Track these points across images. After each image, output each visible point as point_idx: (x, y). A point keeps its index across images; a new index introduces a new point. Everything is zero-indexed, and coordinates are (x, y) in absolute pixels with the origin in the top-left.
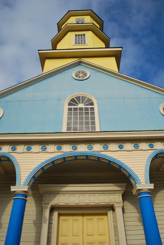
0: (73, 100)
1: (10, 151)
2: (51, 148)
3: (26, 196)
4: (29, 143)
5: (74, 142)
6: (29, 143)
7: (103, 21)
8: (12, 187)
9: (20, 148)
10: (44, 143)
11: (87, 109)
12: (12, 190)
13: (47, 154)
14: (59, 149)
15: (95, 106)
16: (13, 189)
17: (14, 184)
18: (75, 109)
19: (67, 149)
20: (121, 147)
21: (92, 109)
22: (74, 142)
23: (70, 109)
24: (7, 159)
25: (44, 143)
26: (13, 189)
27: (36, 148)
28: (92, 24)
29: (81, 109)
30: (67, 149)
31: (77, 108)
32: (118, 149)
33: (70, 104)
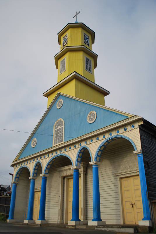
1: (117, 134)
2: (101, 138)
3: (78, 170)
4: (91, 138)
5: (110, 131)
6: (91, 138)
7: (82, 23)
8: (134, 152)
9: (89, 142)
10: (97, 136)
12: (29, 178)
13: (93, 143)
14: (104, 137)
16: (90, 163)
17: (30, 176)
19: (108, 136)
20: (125, 129)
22: (110, 131)
24: (108, 143)
25: (97, 136)
26: (90, 163)
27: (94, 140)
28: (82, 24)
30: (108, 136)
32: (132, 129)
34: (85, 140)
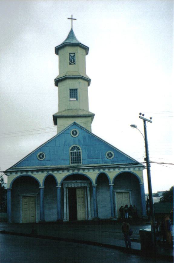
0: (72, 148)
11: (78, 152)
23: (71, 153)
29: (75, 152)
34: (53, 170)
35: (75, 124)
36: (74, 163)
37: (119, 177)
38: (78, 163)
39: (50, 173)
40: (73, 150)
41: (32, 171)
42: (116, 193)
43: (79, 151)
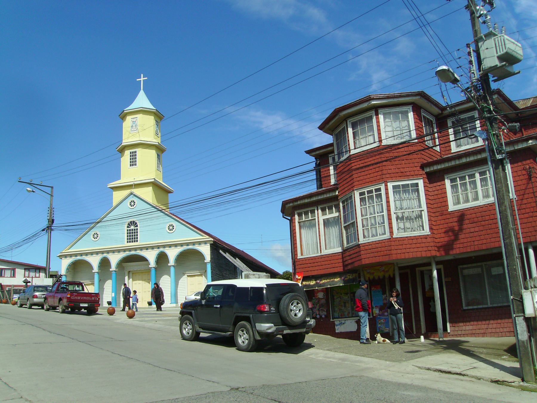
8: (93, 271)
11: (135, 230)
15: (138, 228)
18: (130, 230)
21: (137, 229)
23: (128, 230)
29: (132, 230)
31: (130, 229)
33: (128, 227)
35: (131, 194)
36: (130, 242)
37: (182, 257)
38: (135, 241)
39: (162, 249)
40: (130, 227)
41: (87, 254)
42: (187, 276)
43: (137, 228)
